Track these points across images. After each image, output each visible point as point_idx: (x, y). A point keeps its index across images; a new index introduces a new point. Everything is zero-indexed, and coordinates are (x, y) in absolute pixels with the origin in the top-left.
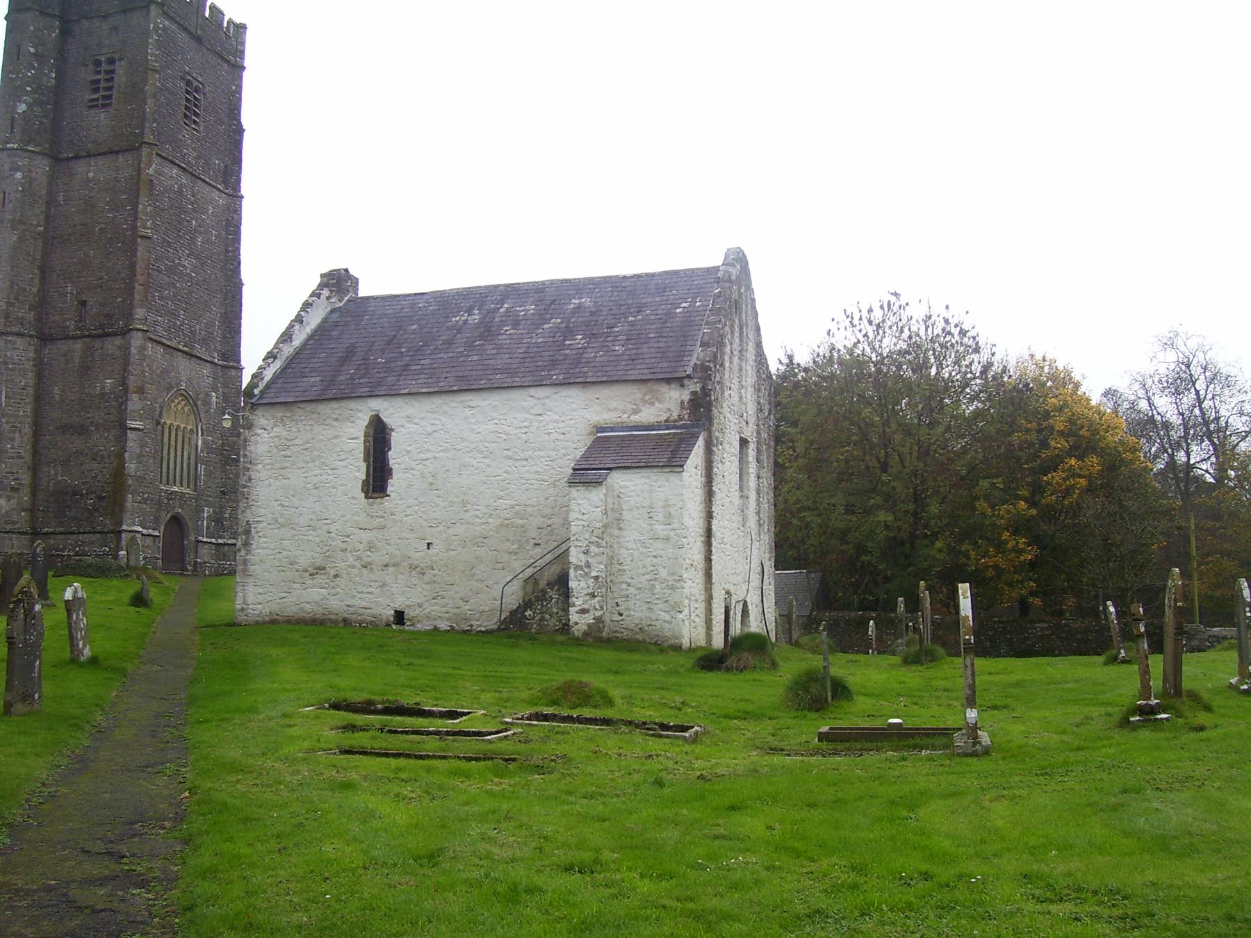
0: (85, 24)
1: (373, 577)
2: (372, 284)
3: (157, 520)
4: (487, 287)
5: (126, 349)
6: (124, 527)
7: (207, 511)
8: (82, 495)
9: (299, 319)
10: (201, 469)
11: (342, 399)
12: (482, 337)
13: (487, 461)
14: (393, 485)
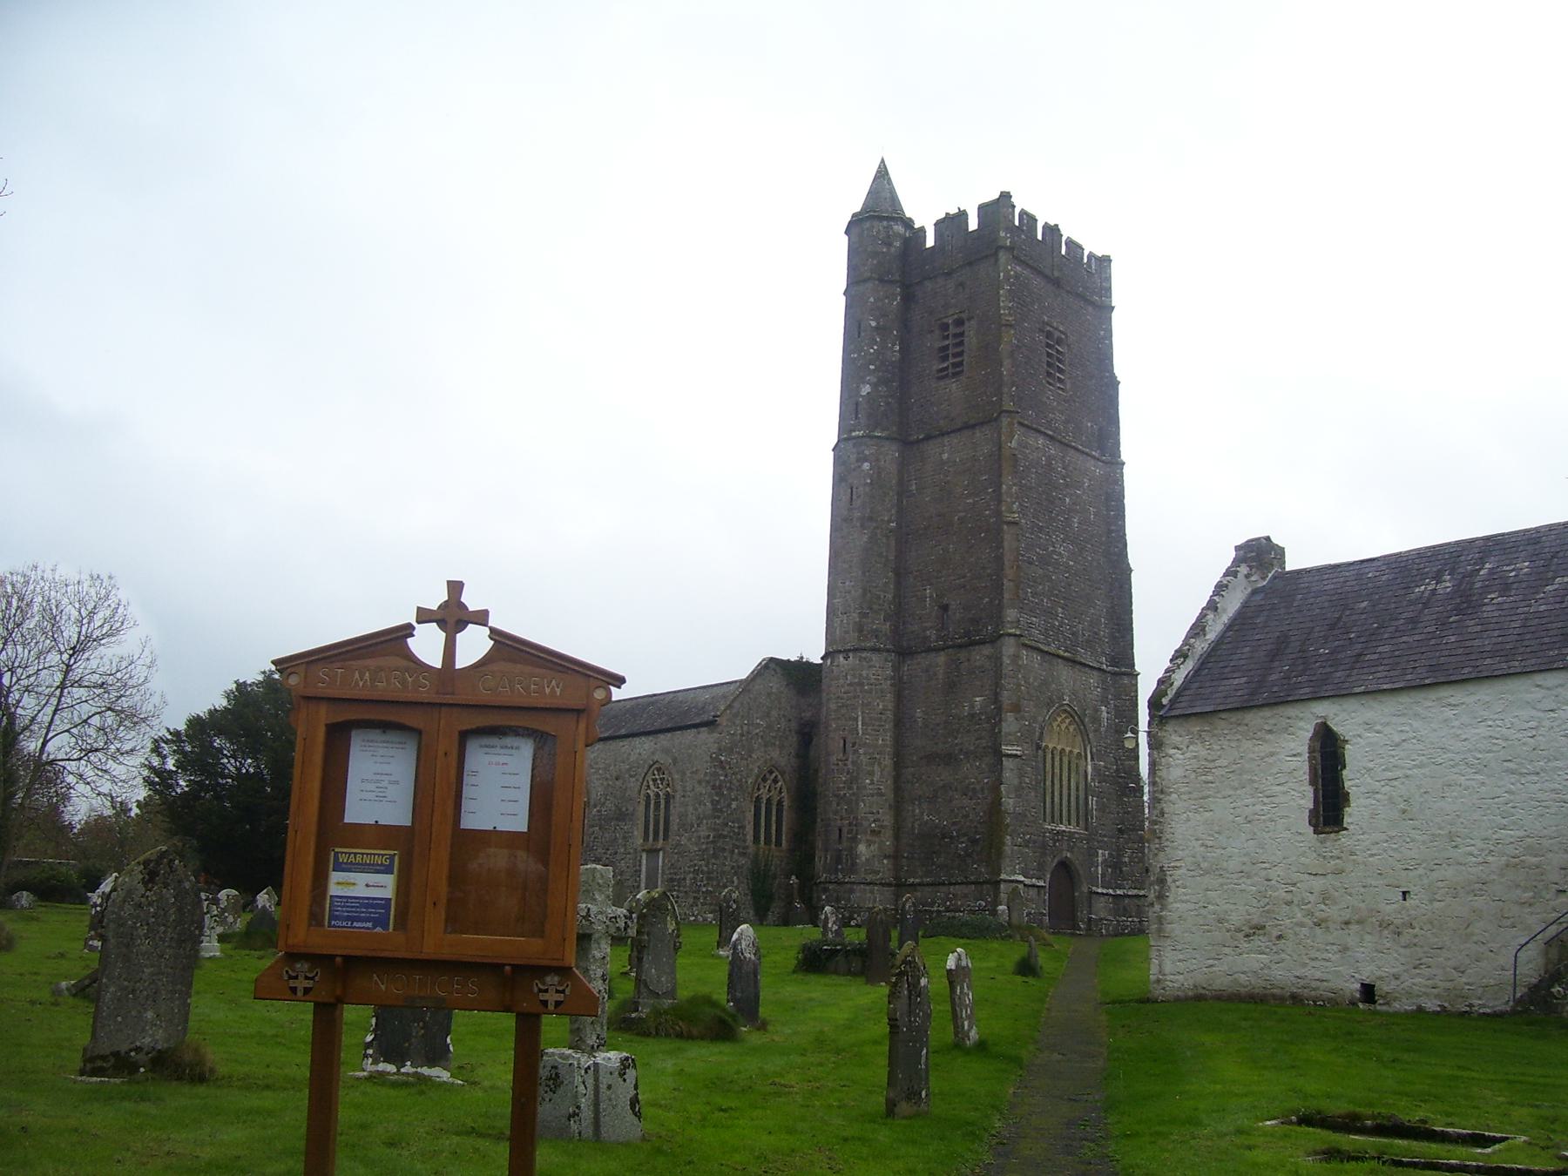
0: (928, 285)
1: (1330, 939)
2: (1304, 553)
3: (1041, 867)
4: (1458, 543)
5: (997, 659)
6: (1003, 876)
7: (1102, 855)
8: (951, 837)
9: (1212, 606)
10: (1093, 802)
11: (1276, 704)
12: (1459, 611)
13: (1478, 777)
14: (1351, 815)
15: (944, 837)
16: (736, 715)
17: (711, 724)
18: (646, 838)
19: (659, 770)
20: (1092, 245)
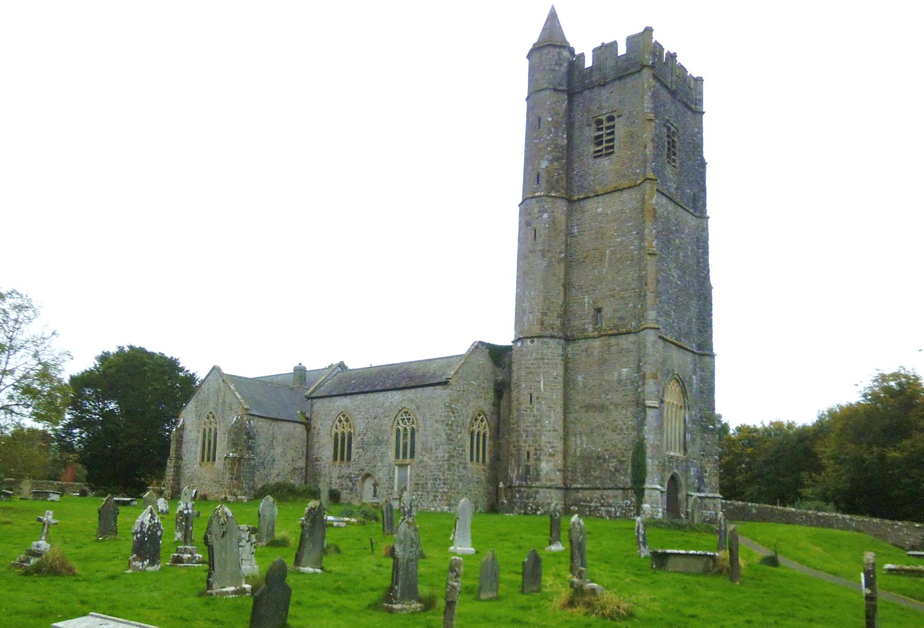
3: (662, 479)
5: (641, 346)
8: (605, 460)
15: (599, 458)
16: (460, 378)
17: (445, 383)
18: (397, 456)
19: (406, 413)
20: (693, 71)
